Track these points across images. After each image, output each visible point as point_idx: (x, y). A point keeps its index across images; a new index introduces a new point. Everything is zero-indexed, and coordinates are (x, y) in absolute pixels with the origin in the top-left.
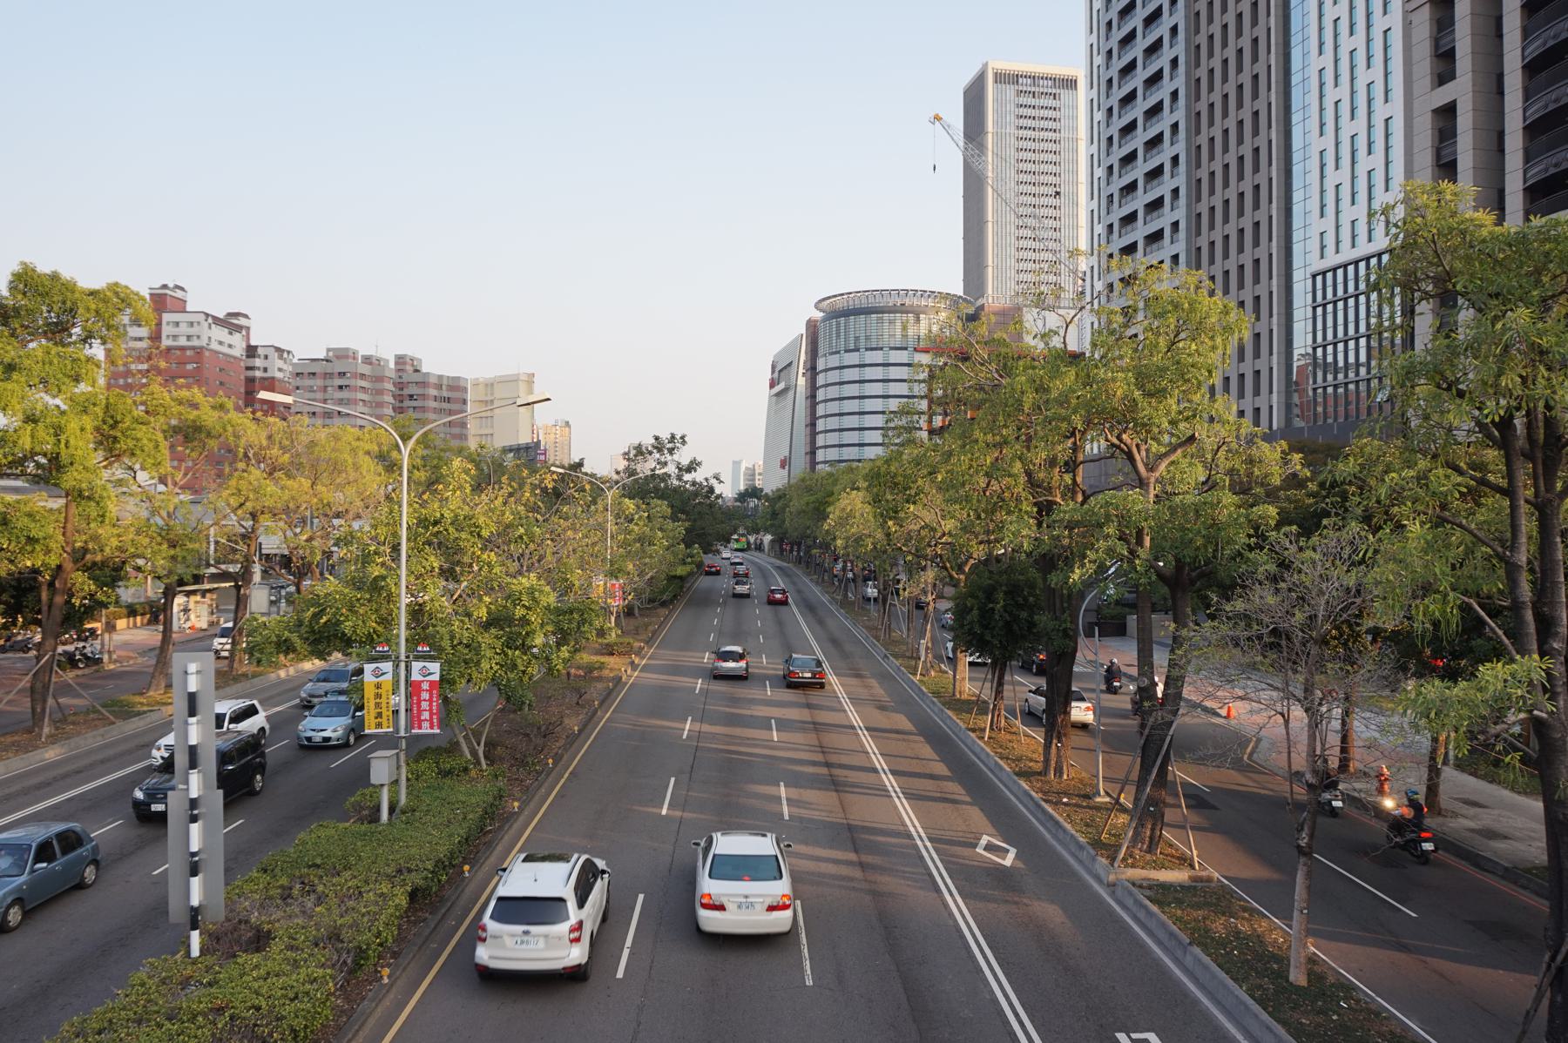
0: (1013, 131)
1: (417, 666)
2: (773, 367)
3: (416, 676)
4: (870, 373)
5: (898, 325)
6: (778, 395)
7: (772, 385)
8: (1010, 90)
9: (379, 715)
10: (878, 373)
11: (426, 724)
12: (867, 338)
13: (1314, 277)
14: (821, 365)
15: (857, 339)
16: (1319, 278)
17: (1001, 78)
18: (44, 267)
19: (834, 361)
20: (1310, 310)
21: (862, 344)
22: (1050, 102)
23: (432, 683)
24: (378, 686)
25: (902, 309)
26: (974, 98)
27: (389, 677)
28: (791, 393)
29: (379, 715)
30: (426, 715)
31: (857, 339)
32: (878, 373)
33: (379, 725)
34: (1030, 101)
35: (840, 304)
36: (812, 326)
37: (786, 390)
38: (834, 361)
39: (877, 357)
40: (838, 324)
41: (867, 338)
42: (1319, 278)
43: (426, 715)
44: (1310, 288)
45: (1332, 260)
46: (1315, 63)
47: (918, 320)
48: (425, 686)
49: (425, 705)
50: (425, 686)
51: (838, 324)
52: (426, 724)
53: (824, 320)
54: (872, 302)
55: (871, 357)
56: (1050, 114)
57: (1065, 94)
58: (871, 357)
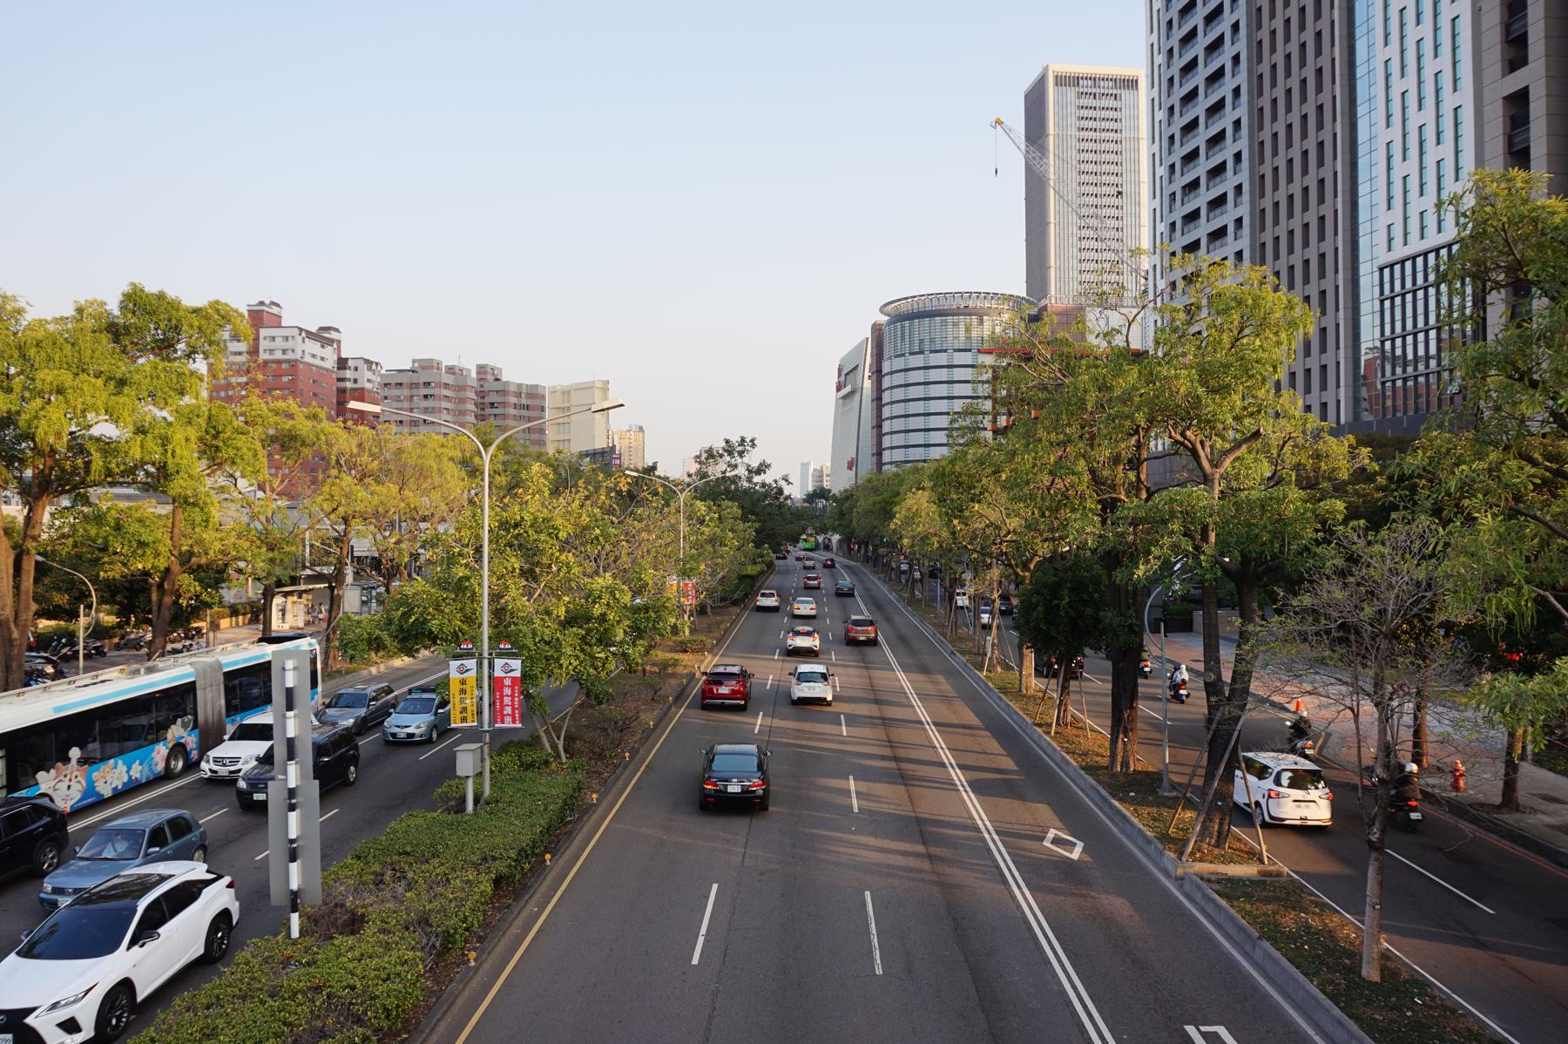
0: (1074, 132)
1: (499, 663)
2: (840, 371)
3: (498, 673)
4: (934, 375)
5: (962, 327)
6: (845, 397)
7: (839, 389)
8: (1071, 93)
9: (465, 709)
10: (942, 375)
11: (508, 719)
12: (932, 341)
13: (1381, 270)
14: (886, 368)
15: (921, 341)
16: (1387, 272)
17: (1063, 81)
18: (151, 288)
19: (899, 363)
20: (1377, 303)
21: (927, 347)
22: (1111, 103)
23: (513, 679)
24: (463, 682)
25: (966, 311)
26: (1035, 101)
27: (473, 673)
28: (857, 397)
29: (465, 709)
30: (508, 710)
31: (921, 341)
32: (942, 375)
33: (464, 720)
34: (1090, 102)
35: (905, 307)
36: (877, 330)
37: (852, 393)
38: (899, 363)
39: (941, 359)
40: (903, 327)
41: (932, 341)
42: (1387, 272)
43: (508, 710)
44: (1377, 281)
45: (1400, 252)
46: (1381, 54)
47: (981, 322)
48: (507, 682)
49: (507, 700)
50: (507, 682)
51: (903, 327)
52: (508, 719)
53: (889, 323)
54: (936, 305)
55: (935, 359)
56: (1112, 114)
57: (1126, 94)
58: (935, 359)
